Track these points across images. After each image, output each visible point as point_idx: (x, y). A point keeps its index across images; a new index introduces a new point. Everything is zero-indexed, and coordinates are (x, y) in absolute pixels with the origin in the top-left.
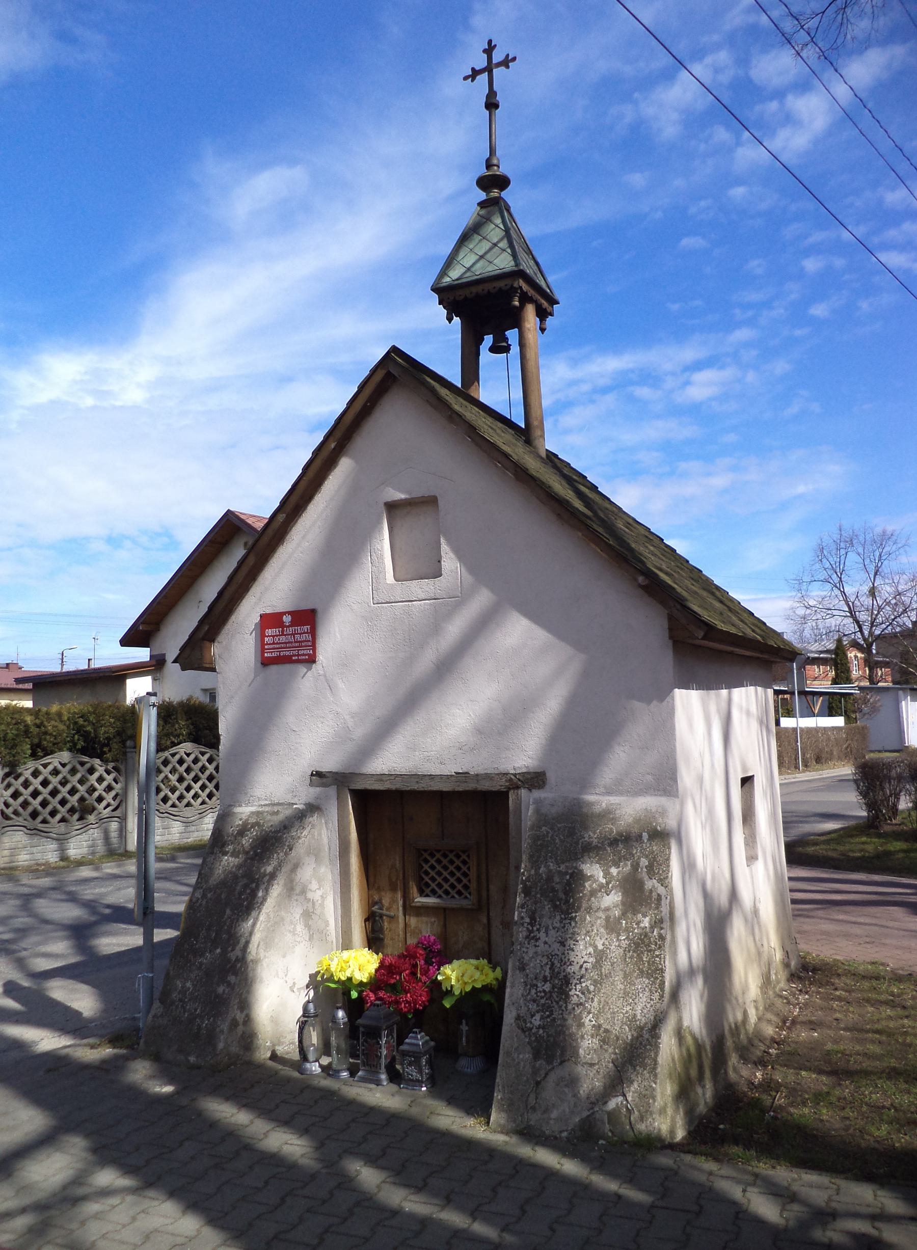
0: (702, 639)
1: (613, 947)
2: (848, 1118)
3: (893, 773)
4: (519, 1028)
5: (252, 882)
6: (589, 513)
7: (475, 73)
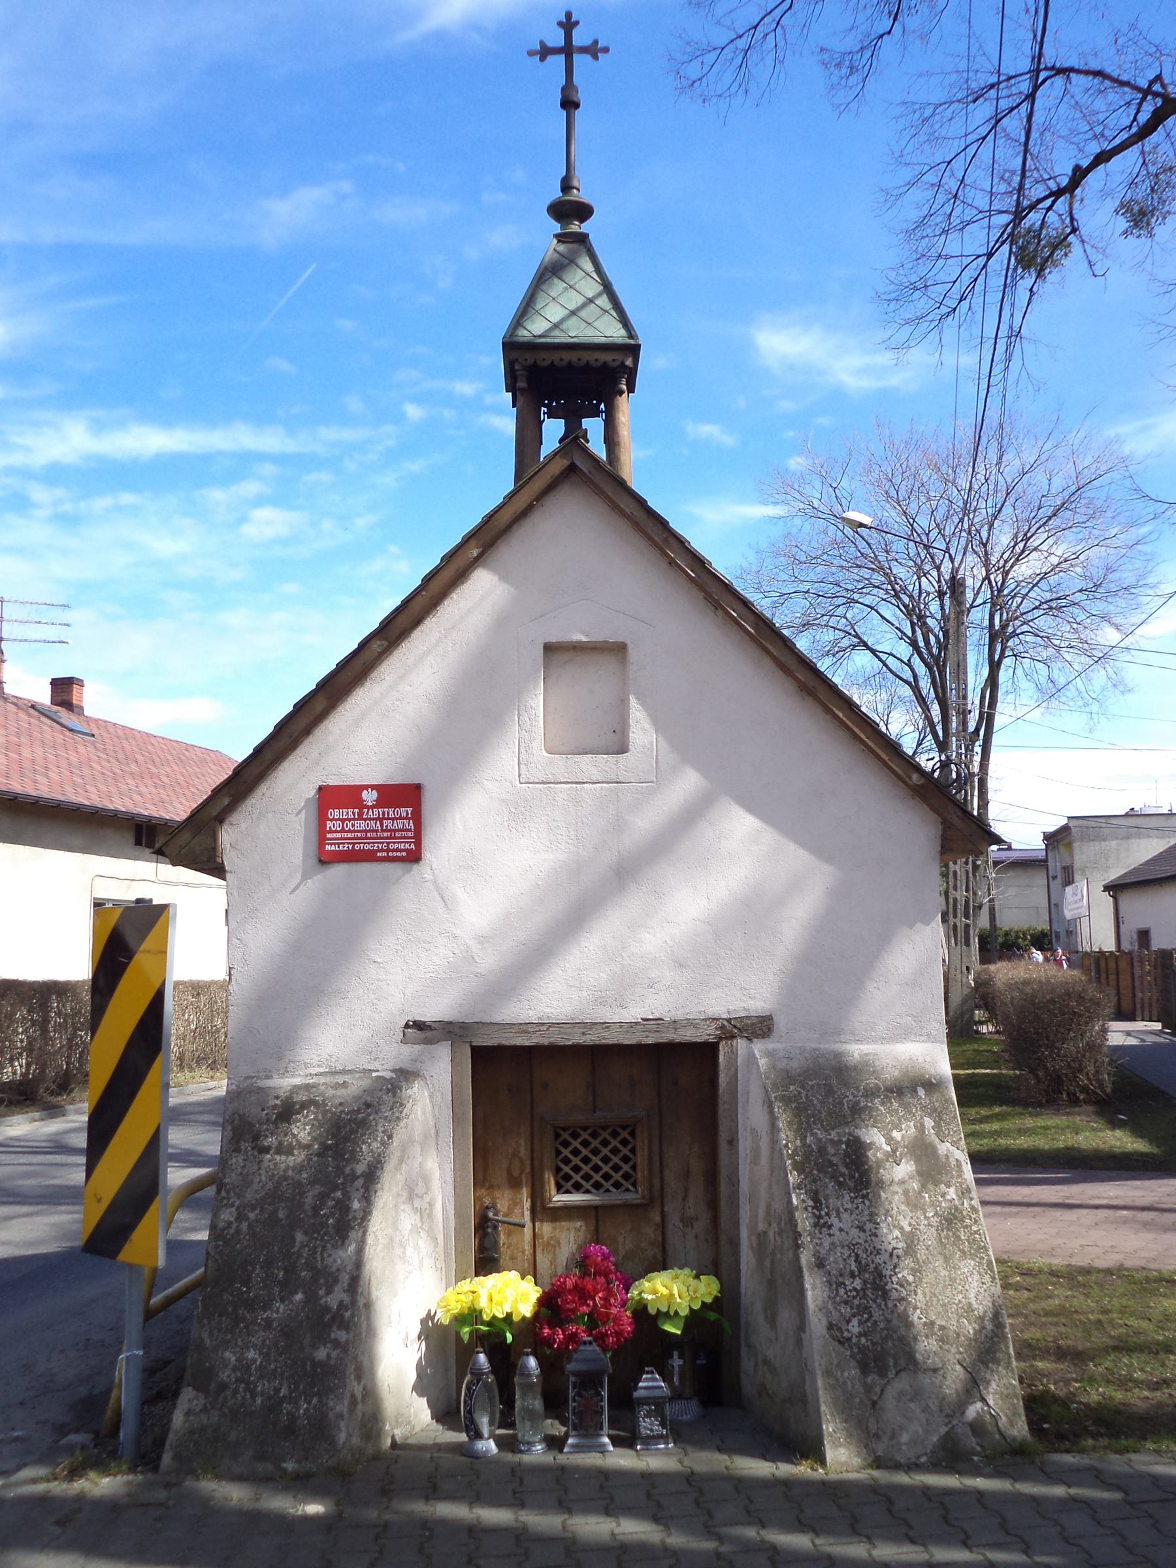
4: (834, 1339)
5: (335, 1188)
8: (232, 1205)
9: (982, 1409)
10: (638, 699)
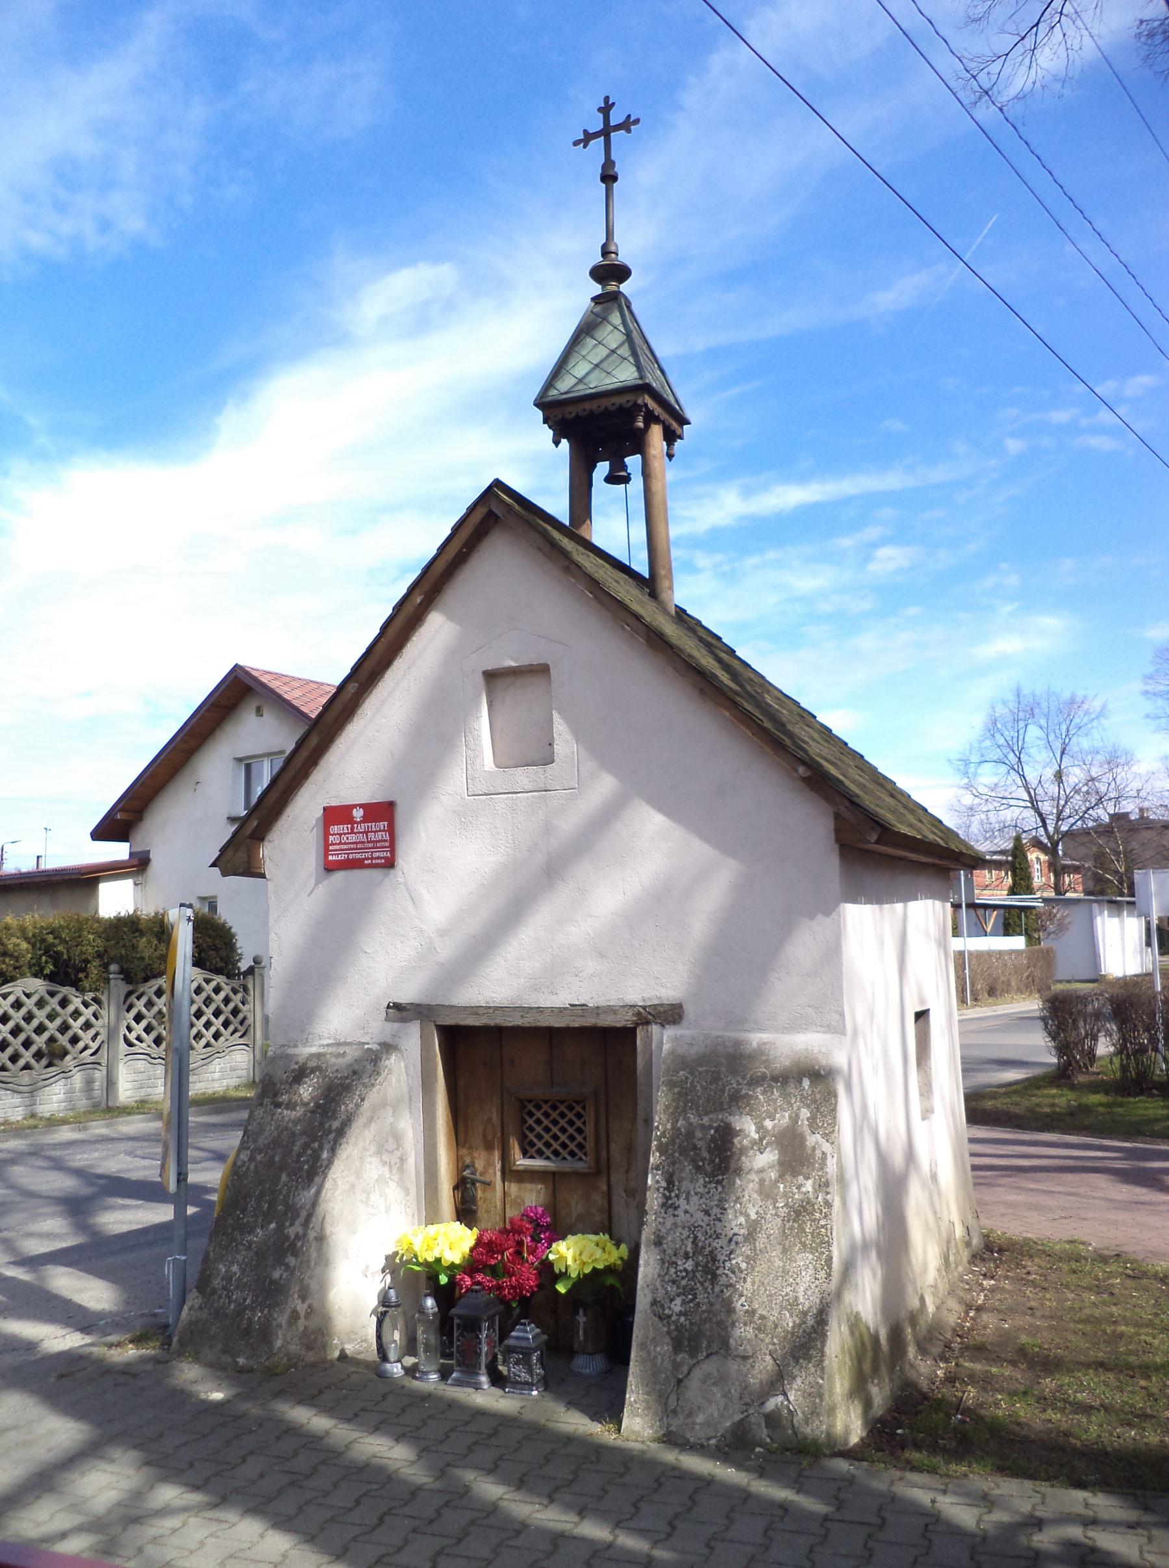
0: (875, 843)
1: (769, 1216)
2: (1050, 1421)
3: (1090, 1008)
4: (655, 1315)
5: (314, 1141)
6: (737, 688)
7: (588, 137)
8: (249, 1148)
9: (782, 1403)
10: (559, 713)
